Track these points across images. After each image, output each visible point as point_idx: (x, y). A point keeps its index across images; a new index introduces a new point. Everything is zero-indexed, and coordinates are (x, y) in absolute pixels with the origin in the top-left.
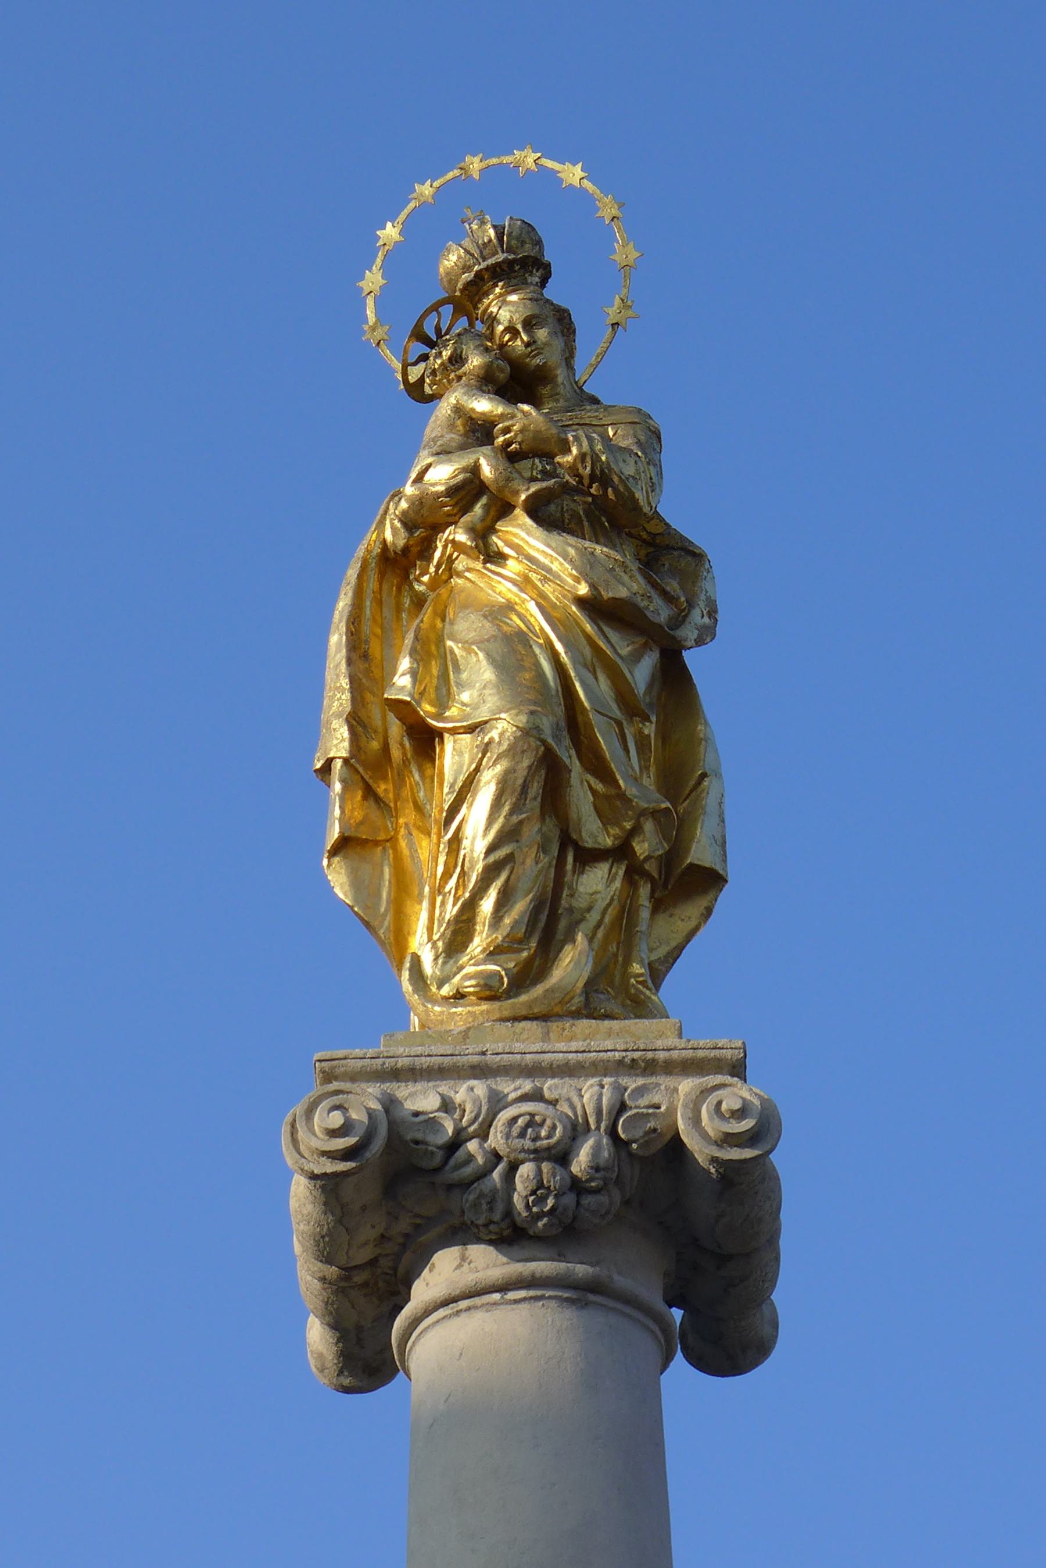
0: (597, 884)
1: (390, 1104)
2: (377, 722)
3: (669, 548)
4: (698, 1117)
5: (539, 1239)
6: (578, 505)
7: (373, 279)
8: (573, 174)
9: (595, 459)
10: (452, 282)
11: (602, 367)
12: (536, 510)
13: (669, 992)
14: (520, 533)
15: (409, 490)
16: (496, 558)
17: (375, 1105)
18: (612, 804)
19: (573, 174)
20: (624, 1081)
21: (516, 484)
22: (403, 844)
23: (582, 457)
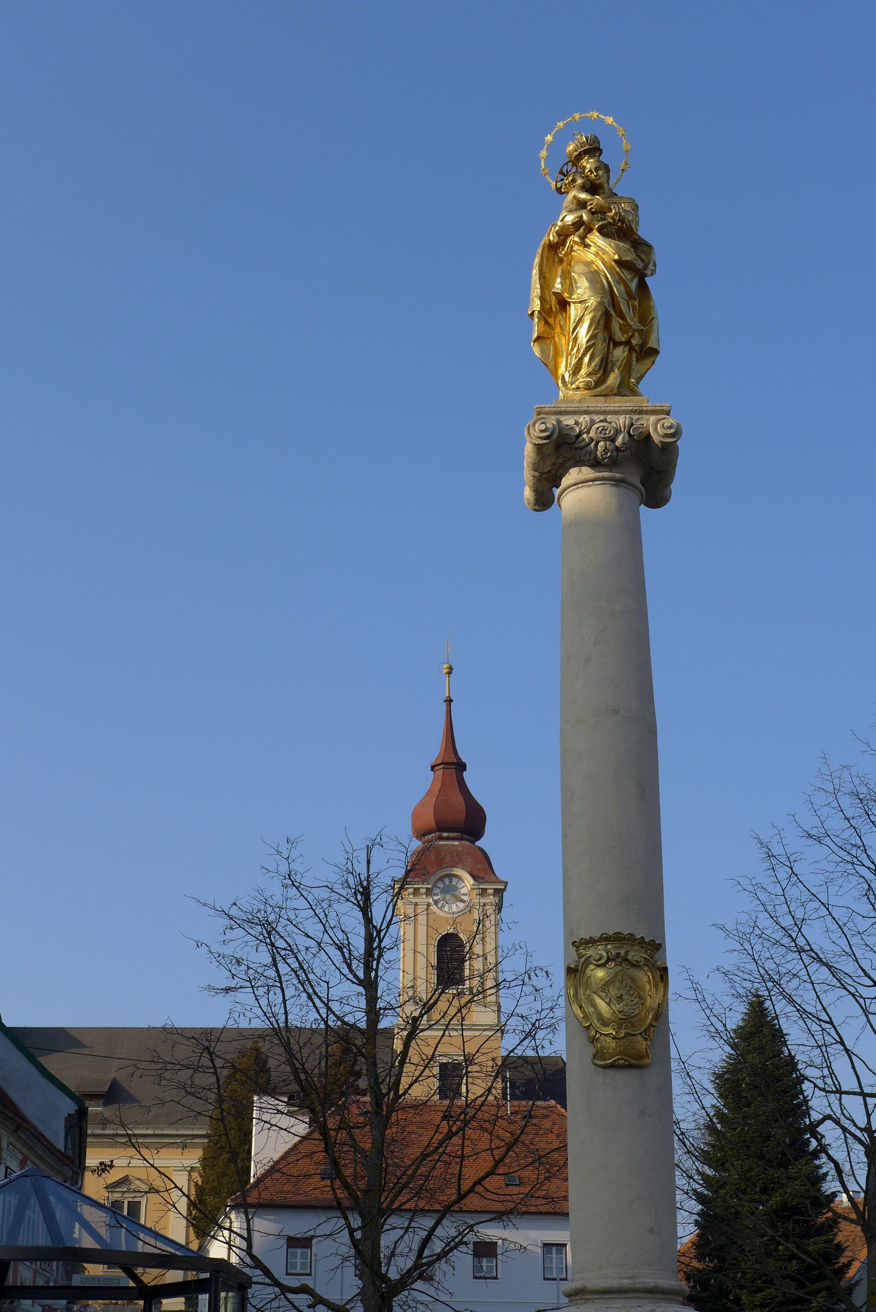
0: (620, 353)
1: (559, 422)
2: (548, 299)
3: (640, 244)
4: (656, 429)
5: (604, 465)
6: (613, 229)
7: (544, 153)
8: (610, 120)
9: (620, 214)
10: (571, 155)
11: (619, 184)
12: (600, 230)
13: (641, 387)
14: (596, 239)
15: (559, 223)
16: (587, 246)
17: (554, 423)
18: (625, 328)
19: (610, 120)
20: (632, 416)
21: (595, 222)
22: (557, 338)
23: (616, 213)
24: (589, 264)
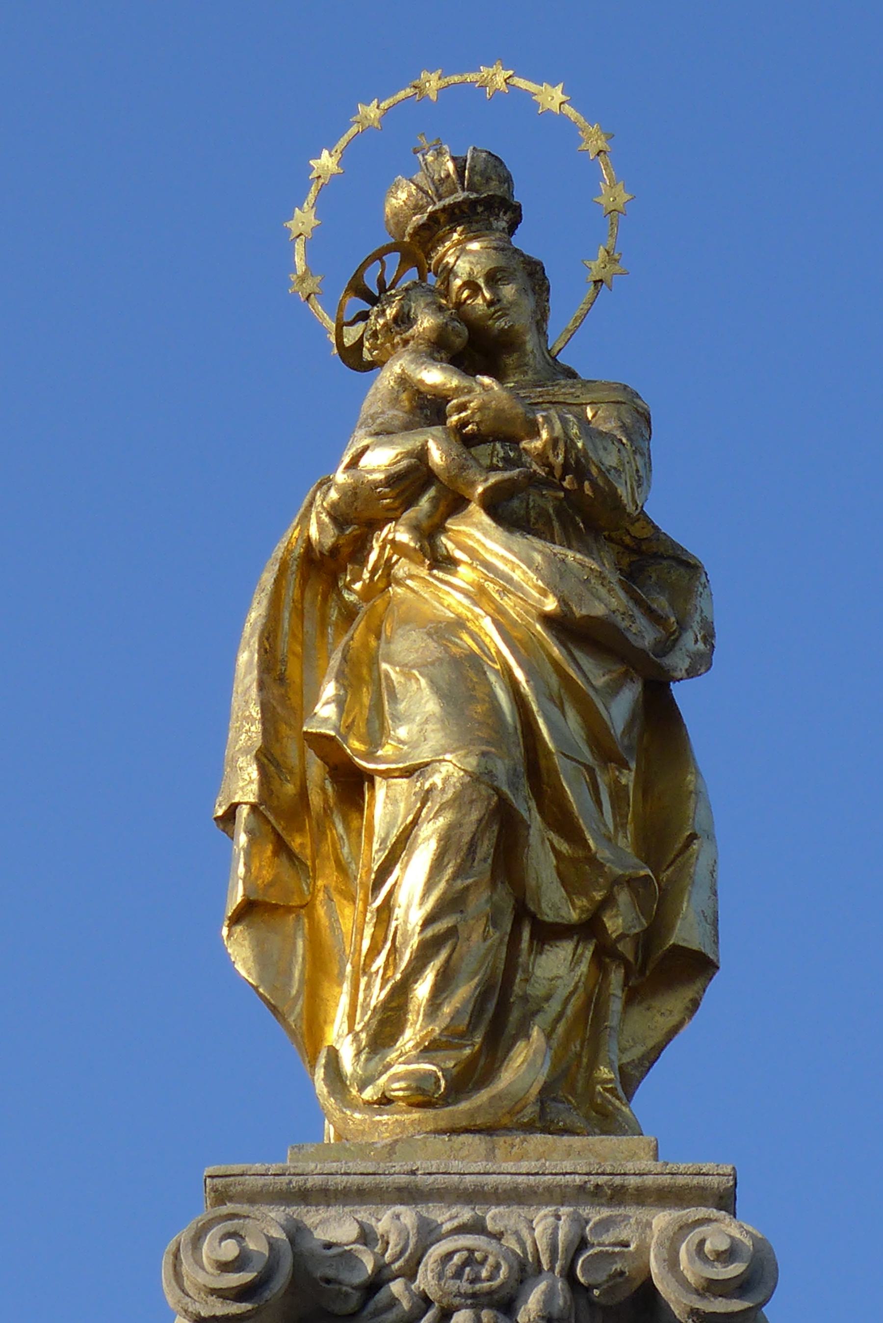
0: (558, 968)
1: (296, 1232)
3: (658, 556)
6: (546, 501)
7: (304, 219)
8: (552, 97)
9: (570, 445)
11: (578, 333)
13: (644, 1103)
14: (476, 534)
15: (341, 477)
17: (278, 1234)
18: (577, 870)
19: (552, 97)
20: (586, 1211)
21: (473, 474)
22: (321, 911)
23: (554, 442)
24: (449, 629)
